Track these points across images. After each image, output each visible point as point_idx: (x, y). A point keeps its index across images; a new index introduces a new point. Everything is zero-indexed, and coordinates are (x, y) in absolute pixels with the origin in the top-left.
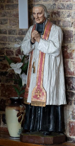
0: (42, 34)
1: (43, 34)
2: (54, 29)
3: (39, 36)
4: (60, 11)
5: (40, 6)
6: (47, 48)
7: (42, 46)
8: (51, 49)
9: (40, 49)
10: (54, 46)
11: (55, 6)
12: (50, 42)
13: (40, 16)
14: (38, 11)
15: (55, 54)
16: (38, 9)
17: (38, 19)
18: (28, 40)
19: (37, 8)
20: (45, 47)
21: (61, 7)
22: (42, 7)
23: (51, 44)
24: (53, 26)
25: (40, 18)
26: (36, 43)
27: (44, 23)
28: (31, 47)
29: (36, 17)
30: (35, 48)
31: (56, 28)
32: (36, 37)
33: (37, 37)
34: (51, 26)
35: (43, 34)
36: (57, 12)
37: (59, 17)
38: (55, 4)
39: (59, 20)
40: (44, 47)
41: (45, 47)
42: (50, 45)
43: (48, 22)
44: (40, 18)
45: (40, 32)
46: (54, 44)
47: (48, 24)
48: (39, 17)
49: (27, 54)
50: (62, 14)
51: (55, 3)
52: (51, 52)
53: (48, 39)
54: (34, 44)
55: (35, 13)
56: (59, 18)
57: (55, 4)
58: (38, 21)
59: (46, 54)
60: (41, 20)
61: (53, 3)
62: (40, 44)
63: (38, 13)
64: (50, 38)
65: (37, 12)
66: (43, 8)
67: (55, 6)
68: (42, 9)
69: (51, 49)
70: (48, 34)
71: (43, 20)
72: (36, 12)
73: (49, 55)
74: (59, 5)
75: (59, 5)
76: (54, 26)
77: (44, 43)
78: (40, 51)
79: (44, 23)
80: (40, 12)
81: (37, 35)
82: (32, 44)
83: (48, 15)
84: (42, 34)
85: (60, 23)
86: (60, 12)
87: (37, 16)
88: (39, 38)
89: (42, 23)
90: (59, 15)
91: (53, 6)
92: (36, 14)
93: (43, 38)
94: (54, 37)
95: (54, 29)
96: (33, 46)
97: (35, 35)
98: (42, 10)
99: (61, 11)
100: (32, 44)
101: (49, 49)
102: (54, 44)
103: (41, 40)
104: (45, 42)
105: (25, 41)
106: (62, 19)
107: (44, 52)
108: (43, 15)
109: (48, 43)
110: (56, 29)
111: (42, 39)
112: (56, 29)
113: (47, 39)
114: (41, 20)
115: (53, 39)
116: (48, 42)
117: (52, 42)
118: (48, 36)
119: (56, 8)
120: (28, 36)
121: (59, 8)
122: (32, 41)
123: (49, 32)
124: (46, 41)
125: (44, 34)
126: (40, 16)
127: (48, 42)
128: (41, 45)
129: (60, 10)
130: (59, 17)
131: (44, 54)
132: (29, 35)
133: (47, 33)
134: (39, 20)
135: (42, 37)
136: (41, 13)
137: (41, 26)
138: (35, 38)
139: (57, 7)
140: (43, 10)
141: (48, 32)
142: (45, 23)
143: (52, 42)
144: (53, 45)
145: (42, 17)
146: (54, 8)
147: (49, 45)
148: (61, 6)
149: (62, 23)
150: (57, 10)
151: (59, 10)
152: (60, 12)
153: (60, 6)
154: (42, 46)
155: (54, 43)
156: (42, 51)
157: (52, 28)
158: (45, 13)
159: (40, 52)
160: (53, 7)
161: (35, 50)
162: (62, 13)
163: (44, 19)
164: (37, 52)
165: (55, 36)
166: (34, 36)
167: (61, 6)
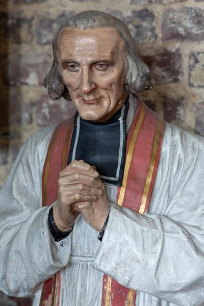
0: (112, 179)
1: (119, 183)
2: (180, 150)
3: (100, 192)
4: (178, 50)
5: (104, 22)
6: (153, 262)
7: (120, 251)
8: (175, 267)
9: (108, 268)
10: (194, 253)
11: (145, 24)
12: (168, 225)
13: (105, 78)
14: (95, 53)
15: (192, 292)
16: (91, 40)
17: (91, 97)
18: (22, 211)
19: (86, 35)
20: (139, 255)
21: (186, 29)
22: (112, 29)
23: (175, 242)
24: (168, 134)
25: (103, 93)
26: (82, 232)
27: (121, 120)
28: (54, 258)
29: (86, 88)
30: (75, 258)
31: (190, 145)
32: (85, 197)
33: (91, 201)
34: (161, 136)
35: (119, 183)
36: (163, 54)
37: (176, 80)
38: (147, 11)
39: (172, 95)
40: (135, 259)
41: (139, 255)
42: (166, 245)
43: (142, 114)
44: (103, 93)
45: (107, 172)
46: (190, 238)
47: (142, 127)
48: (97, 86)
49: (18, 292)
50: (191, 68)
51: (150, 8)
52: (176, 285)
53: (148, 208)
54: (69, 237)
55: (78, 60)
56: (173, 85)
57: (146, 14)
58: (93, 107)
59: (141, 294)
60: (106, 103)
61: (138, 7)
62: (113, 240)
63: (92, 65)
64: (159, 203)
65: (90, 59)
66: (121, 34)
67: (145, 24)
68: (115, 37)
69: (172, 270)
70: (149, 180)
71: (117, 104)
72: (84, 60)
73: (155, 299)
74: (171, 15)
75: (171, 15)
76: (177, 136)
77: (135, 234)
78: (105, 276)
79: (121, 120)
80: (107, 55)
81: (93, 190)
82: (58, 235)
83: (145, 75)
84: (112, 179)
85: (181, 111)
86: (178, 54)
87: (91, 82)
88: (101, 202)
89: (110, 119)
90: (175, 74)
91: (138, 21)
92: (86, 68)
93: (120, 202)
94: (186, 199)
95: (180, 150)
96: (64, 248)
97: (80, 187)
98: (117, 47)
99: (186, 48)
100: (58, 235)
101: (161, 269)
102: (190, 238)
103: (117, 219)
104: (138, 227)
105: (10, 218)
106: (194, 90)
107: (133, 286)
108: (122, 75)
109: (158, 233)
110: (190, 149)
111: (120, 209)
112: (190, 149)
113: (142, 210)
114: (108, 104)
115: (180, 210)
116: (156, 227)
117: (178, 223)
118: (147, 189)
119: (156, 36)
120: (23, 192)
121: (176, 36)
122: (59, 223)
123: (152, 168)
124: (144, 221)
125: (124, 182)
126: (105, 78)
127: (156, 227)
128: (117, 249)
129: (178, 45)
130: (176, 80)
131: (130, 296)
132: (28, 185)
133: (141, 175)
134: (98, 101)
135: (113, 197)
136: (107, 65)
137: (101, 134)
138: (80, 206)
139: (159, 31)
140: (122, 44)
141: (148, 170)
142: (125, 119)
143: (179, 230)
144: (189, 246)
145: (114, 87)
146: (139, 34)
147: (163, 246)
148: (189, 24)
149: (193, 114)
150: (160, 43)
151: (173, 46)
152: (180, 55)
153: (179, 23)
154: (125, 250)
155: (190, 230)
156: (122, 280)
157: (166, 149)
158: (131, 62)
159: (105, 283)
160: (137, 27)
161: (77, 271)
162: (197, 61)
163: (120, 94)
164: (84, 281)
165: (192, 194)
166: (77, 196)
167: (189, 24)
